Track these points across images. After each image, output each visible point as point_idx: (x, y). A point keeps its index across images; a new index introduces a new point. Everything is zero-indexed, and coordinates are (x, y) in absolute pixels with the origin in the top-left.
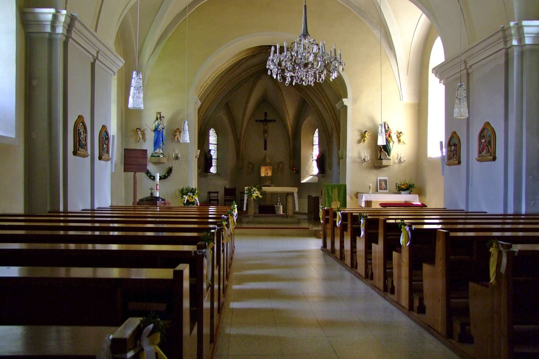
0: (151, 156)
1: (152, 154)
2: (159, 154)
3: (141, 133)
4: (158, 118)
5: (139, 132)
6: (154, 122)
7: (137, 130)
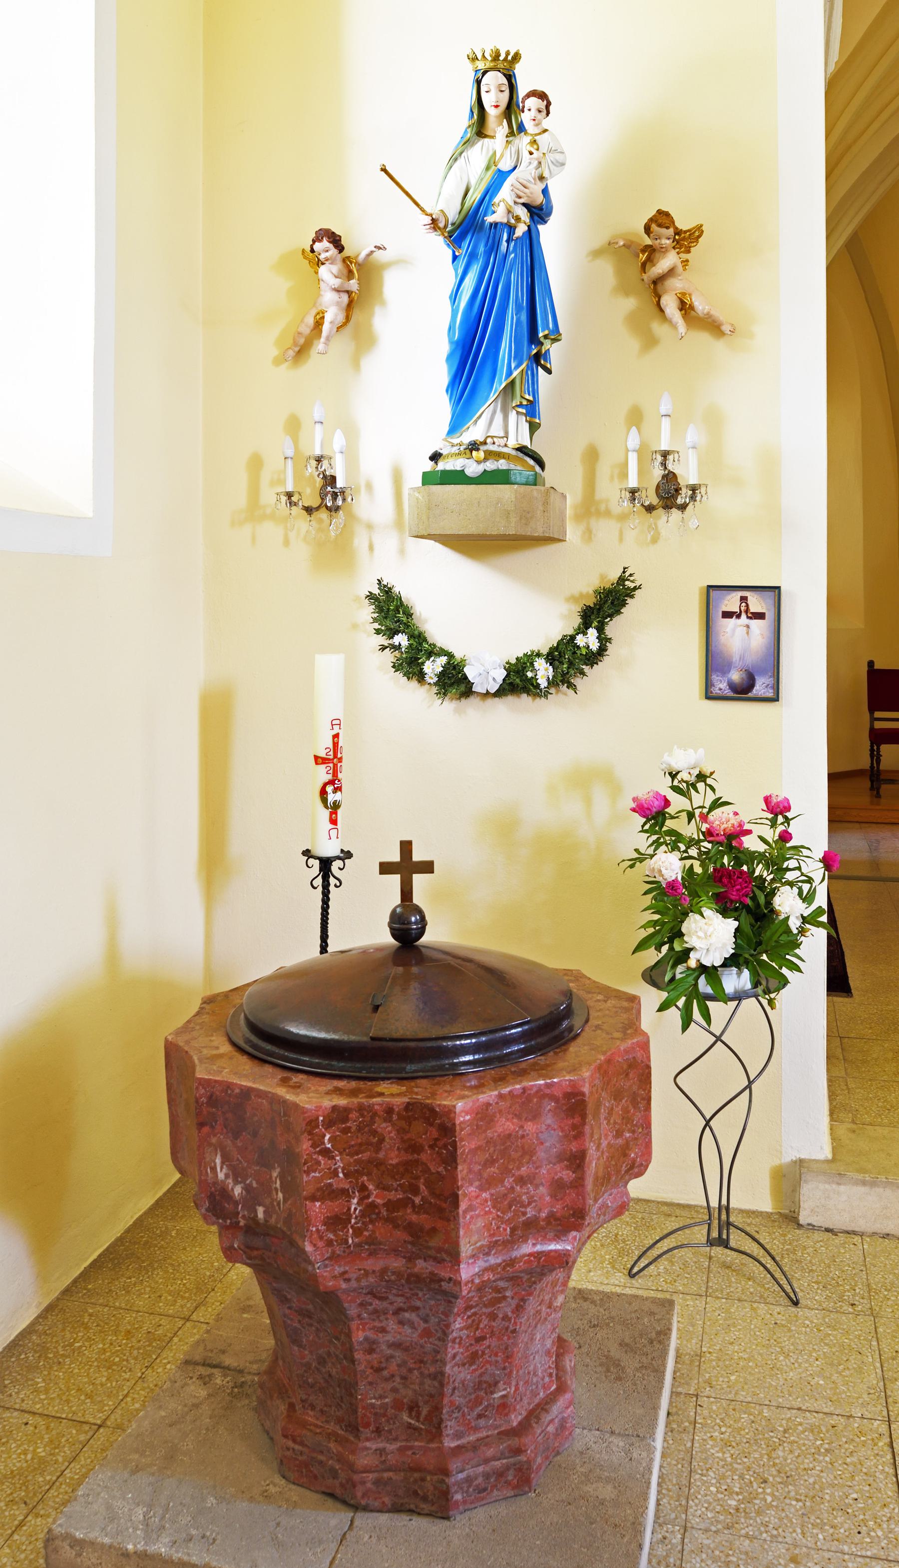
0: (428, 479)
1: (435, 457)
2: (498, 455)
3: (336, 283)
4: (492, 113)
5: (323, 271)
6: (454, 159)
7: (318, 246)
